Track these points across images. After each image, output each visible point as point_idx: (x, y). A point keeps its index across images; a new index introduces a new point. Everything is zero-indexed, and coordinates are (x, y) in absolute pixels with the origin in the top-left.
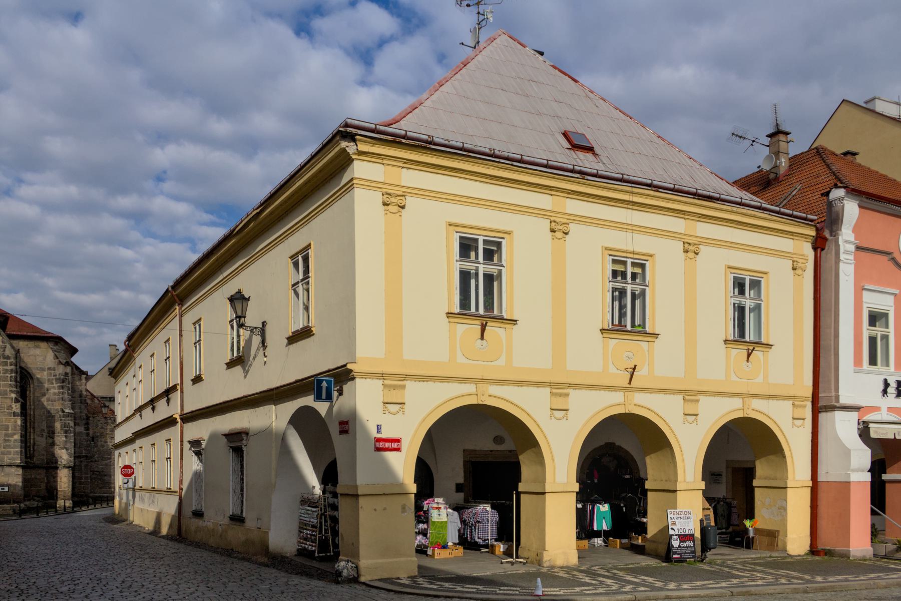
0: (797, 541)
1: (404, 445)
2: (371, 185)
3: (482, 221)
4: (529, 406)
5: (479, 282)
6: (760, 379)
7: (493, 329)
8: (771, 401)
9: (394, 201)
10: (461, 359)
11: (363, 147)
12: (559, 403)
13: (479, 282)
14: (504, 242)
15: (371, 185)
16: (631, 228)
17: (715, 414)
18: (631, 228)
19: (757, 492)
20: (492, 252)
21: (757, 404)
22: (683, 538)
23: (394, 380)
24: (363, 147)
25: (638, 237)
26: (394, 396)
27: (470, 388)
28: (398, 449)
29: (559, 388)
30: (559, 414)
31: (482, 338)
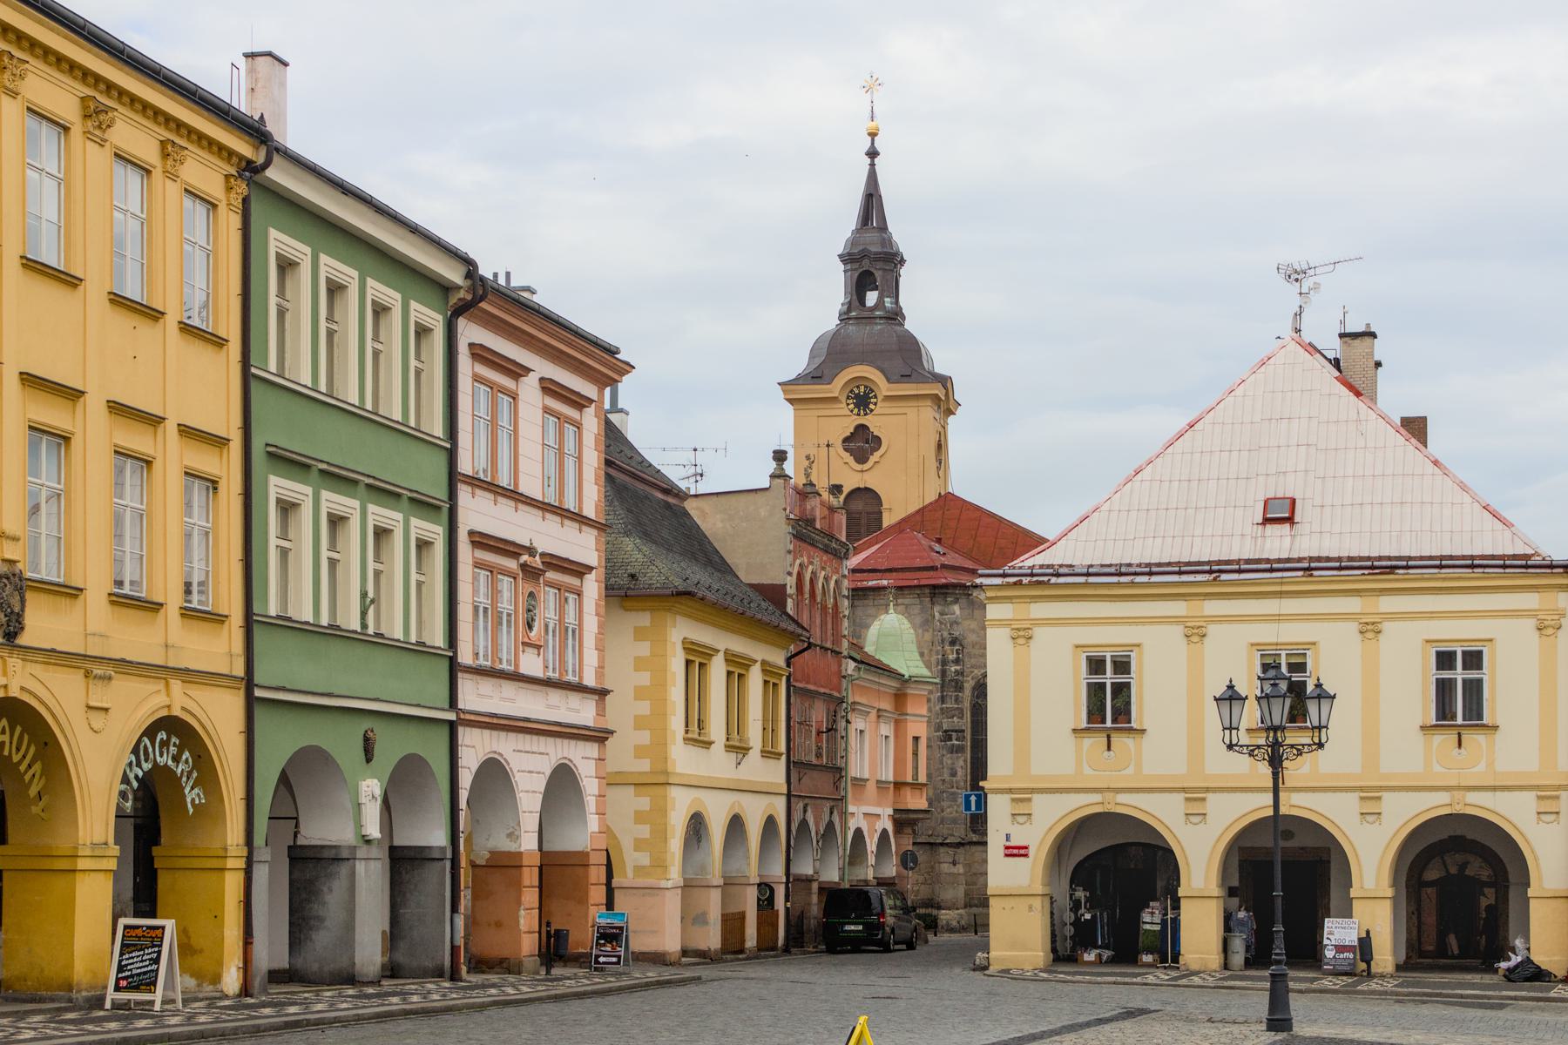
0: (369, 952)
1: (1032, 852)
2: (1001, 623)
3: (1107, 638)
4: (1164, 815)
5: (1109, 701)
6: (1481, 767)
7: (1473, 739)
8: (1498, 794)
9: (1022, 635)
10: (1087, 771)
11: (990, 594)
12: (1370, 807)
13: (1109, 701)
14: (1485, 651)
15: (1001, 623)
16: (1278, 618)
17: (1405, 813)
18: (1278, 618)
19: (1533, 904)
20: (1474, 659)
21: (1472, 797)
22: (1340, 949)
23: (1021, 796)
24: (990, 594)
25: (1284, 626)
26: (1022, 809)
27: (1097, 798)
28: (1026, 855)
29: (1370, 794)
30: (1020, 819)
31: (1109, 748)
